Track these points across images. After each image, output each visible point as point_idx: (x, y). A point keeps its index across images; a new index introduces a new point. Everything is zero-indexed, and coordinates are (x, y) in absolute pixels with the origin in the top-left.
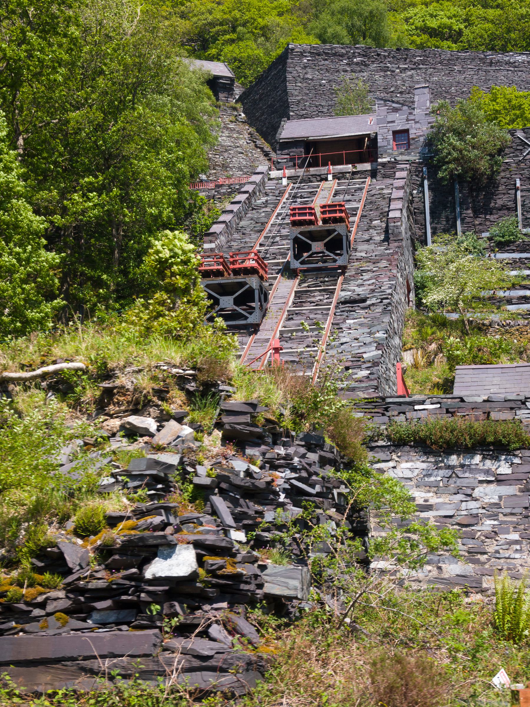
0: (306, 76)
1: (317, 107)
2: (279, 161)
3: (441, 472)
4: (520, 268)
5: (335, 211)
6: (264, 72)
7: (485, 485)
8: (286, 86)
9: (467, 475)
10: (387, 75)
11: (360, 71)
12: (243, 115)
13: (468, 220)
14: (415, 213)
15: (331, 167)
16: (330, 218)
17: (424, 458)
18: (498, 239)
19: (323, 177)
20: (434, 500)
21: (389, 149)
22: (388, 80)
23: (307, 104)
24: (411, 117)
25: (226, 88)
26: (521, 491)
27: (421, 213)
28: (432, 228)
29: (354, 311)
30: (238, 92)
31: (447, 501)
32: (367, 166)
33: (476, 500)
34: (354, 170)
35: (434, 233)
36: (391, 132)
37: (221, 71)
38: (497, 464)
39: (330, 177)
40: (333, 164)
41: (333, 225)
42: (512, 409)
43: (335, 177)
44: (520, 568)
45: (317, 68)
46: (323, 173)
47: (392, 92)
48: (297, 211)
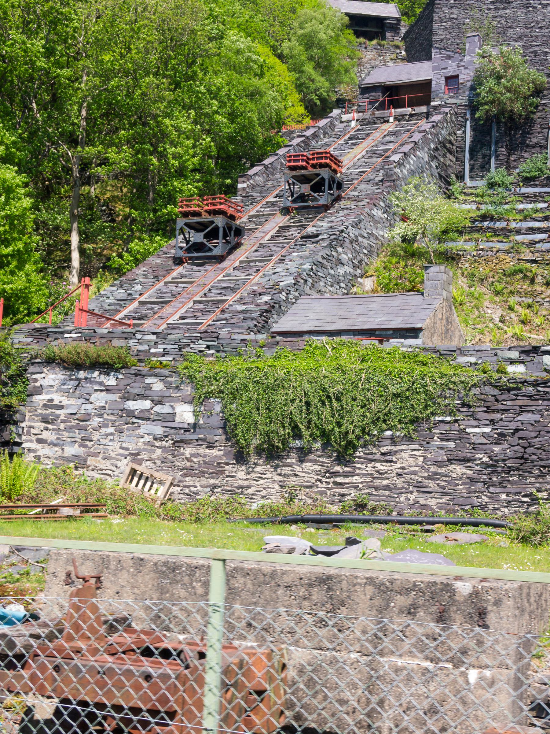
0: (452, 16)
1: (458, 45)
2: (360, 104)
3: (72, 383)
4: (535, 202)
5: (322, 158)
6: (433, 11)
7: (99, 393)
8: (432, 26)
9: (88, 385)
10: (529, 11)
11: (503, 9)
12: (404, 53)
13: (501, 157)
14: (457, 151)
15: (393, 110)
16: (317, 164)
17: (63, 372)
18: (524, 174)
19: (386, 119)
20: (65, 401)
21: (441, 93)
22: (529, 16)
23: (450, 42)
24: (462, 64)
25: (393, 28)
26: (120, 398)
27: (462, 151)
28: (470, 165)
29: (305, 245)
30: (403, 30)
31: (73, 403)
32: (423, 109)
33: (92, 403)
34: (413, 112)
35: (471, 170)
36: (443, 78)
37: (389, 12)
38: (107, 378)
39: (391, 119)
40: (395, 108)
41: (319, 170)
42: (126, 338)
43: (396, 119)
44: (111, 452)
45: (463, 8)
46: (386, 115)
47: (532, 27)
48: (292, 158)
